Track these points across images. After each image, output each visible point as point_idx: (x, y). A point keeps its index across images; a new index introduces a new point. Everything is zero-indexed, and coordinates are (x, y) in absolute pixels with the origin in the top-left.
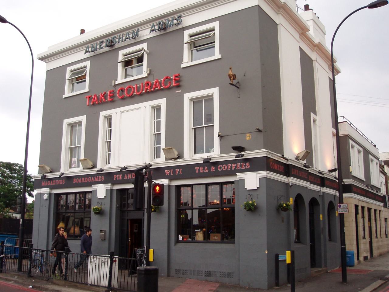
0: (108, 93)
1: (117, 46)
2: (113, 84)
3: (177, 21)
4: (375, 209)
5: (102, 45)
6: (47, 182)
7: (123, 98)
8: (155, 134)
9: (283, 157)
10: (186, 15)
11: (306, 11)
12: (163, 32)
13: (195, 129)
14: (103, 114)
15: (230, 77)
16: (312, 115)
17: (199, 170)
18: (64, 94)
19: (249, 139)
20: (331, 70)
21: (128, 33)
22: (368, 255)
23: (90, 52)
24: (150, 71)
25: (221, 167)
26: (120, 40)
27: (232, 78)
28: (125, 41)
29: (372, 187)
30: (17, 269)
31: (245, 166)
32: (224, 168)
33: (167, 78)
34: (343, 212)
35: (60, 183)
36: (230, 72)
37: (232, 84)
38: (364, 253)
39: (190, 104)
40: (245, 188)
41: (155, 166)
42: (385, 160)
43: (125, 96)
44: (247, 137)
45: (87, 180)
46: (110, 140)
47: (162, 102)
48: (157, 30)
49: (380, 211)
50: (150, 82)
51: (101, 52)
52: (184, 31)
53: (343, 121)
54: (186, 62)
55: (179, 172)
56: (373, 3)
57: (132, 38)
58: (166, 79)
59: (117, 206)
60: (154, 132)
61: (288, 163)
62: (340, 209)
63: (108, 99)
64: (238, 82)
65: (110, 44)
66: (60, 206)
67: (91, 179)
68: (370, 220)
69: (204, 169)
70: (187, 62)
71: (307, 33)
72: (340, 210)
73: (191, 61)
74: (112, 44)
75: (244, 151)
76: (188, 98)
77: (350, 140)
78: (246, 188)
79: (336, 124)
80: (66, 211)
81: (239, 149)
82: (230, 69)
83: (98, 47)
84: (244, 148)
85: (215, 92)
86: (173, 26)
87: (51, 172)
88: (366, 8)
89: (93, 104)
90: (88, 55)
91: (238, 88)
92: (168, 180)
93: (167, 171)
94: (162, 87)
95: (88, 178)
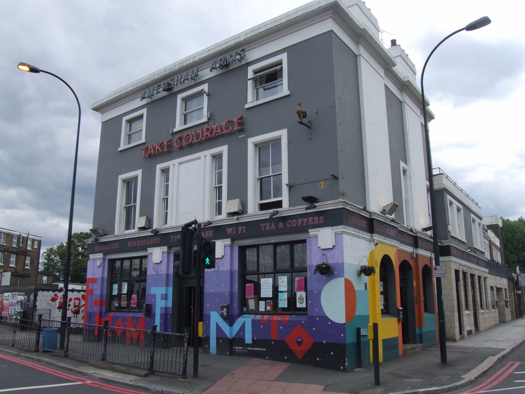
0: (165, 142)
1: (175, 89)
2: (171, 133)
3: (240, 55)
4: (479, 275)
5: (159, 89)
6: (101, 247)
7: (181, 148)
8: (216, 187)
9: (365, 209)
10: (251, 48)
11: (392, 47)
12: (224, 70)
13: (261, 179)
14: (159, 167)
15: (299, 115)
16: (402, 164)
17: (265, 227)
18: (119, 147)
19: (323, 188)
20: (422, 115)
21: (187, 74)
22: (473, 328)
23: (147, 98)
24: (211, 114)
25: (291, 223)
26: (179, 82)
27: (301, 116)
28: (183, 82)
29: (474, 249)
30: (59, 348)
31: (319, 220)
32: (294, 223)
33: (229, 122)
34: (440, 276)
35: (114, 246)
36: (299, 108)
37: (301, 123)
38: (468, 326)
39: (255, 150)
40: (319, 246)
41: (215, 224)
42: (489, 224)
43: (183, 145)
44: (320, 186)
45: (142, 243)
46: (167, 197)
47: (224, 149)
48: (218, 67)
49: (485, 278)
50: (211, 127)
51: (159, 98)
52: (248, 67)
53: (439, 173)
54: (251, 101)
55: (242, 230)
56: (471, 23)
57: (192, 78)
58: (228, 122)
59: (175, 272)
60: (216, 185)
61: (371, 218)
62: (436, 272)
63: (165, 149)
64: (310, 121)
65: (168, 87)
66: (114, 273)
67: (147, 241)
68: (473, 287)
69: (270, 226)
70: (252, 102)
71: (393, 68)
72: (436, 273)
73: (257, 101)
74: (170, 87)
75: (317, 202)
76: (253, 143)
77: (447, 195)
78: (320, 247)
79: (430, 176)
80: (121, 279)
81: (311, 200)
82: (299, 105)
83: (155, 92)
84: (317, 199)
85: (283, 134)
86: (235, 61)
87: (105, 235)
88: (463, 31)
89: (150, 156)
90: (144, 102)
91: (310, 128)
92: (230, 240)
93: (229, 229)
94: (224, 132)
95: (143, 241)
